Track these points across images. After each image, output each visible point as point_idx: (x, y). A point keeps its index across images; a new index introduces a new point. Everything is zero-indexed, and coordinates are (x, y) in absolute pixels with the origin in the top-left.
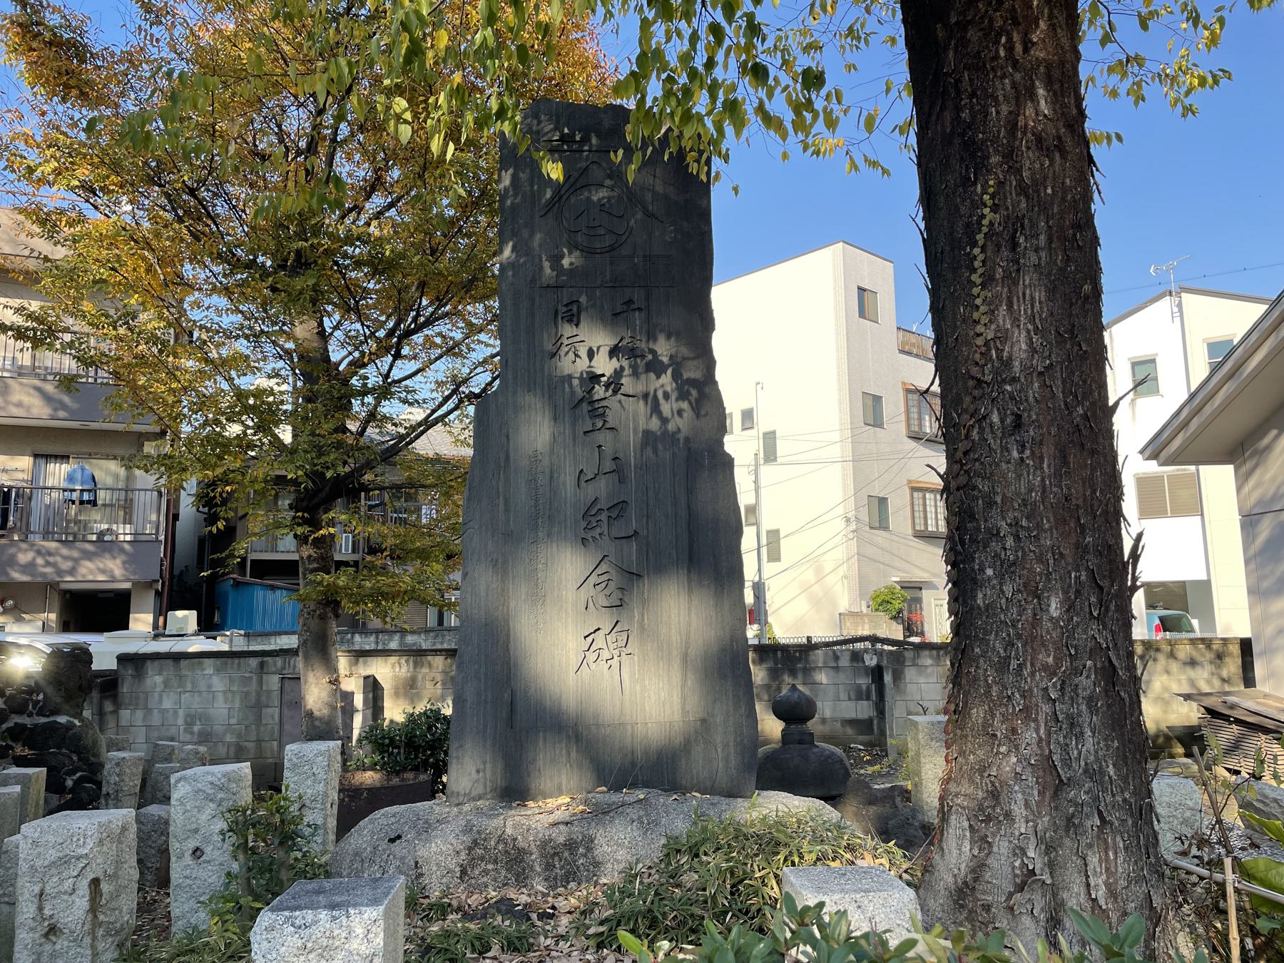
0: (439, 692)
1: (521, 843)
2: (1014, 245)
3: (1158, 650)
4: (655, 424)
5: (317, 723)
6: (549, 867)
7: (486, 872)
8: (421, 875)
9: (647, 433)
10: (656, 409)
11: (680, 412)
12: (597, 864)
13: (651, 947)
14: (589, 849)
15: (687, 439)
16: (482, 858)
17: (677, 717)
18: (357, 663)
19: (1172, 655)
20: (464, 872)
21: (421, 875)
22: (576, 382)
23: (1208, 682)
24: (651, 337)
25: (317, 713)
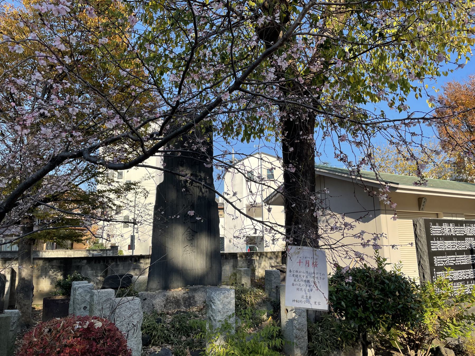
0: (40, 273)
1: (178, 298)
2: (306, 175)
3: (263, 255)
4: (201, 194)
5: (26, 282)
6: (185, 303)
7: (171, 305)
8: (154, 308)
9: (199, 196)
10: (201, 190)
11: (206, 191)
12: (196, 302)
13: (337, 265)
14: (194, 298)
15: (208, 198)
16: (169, 302)
17: (205, 267)
18: (5, 263)
19: (266, 256)
20: (165, 306)
21: (154, 308)
22: (183, 182)
23: (274, 264)
24: (200, 172)
25: (26, 278)
